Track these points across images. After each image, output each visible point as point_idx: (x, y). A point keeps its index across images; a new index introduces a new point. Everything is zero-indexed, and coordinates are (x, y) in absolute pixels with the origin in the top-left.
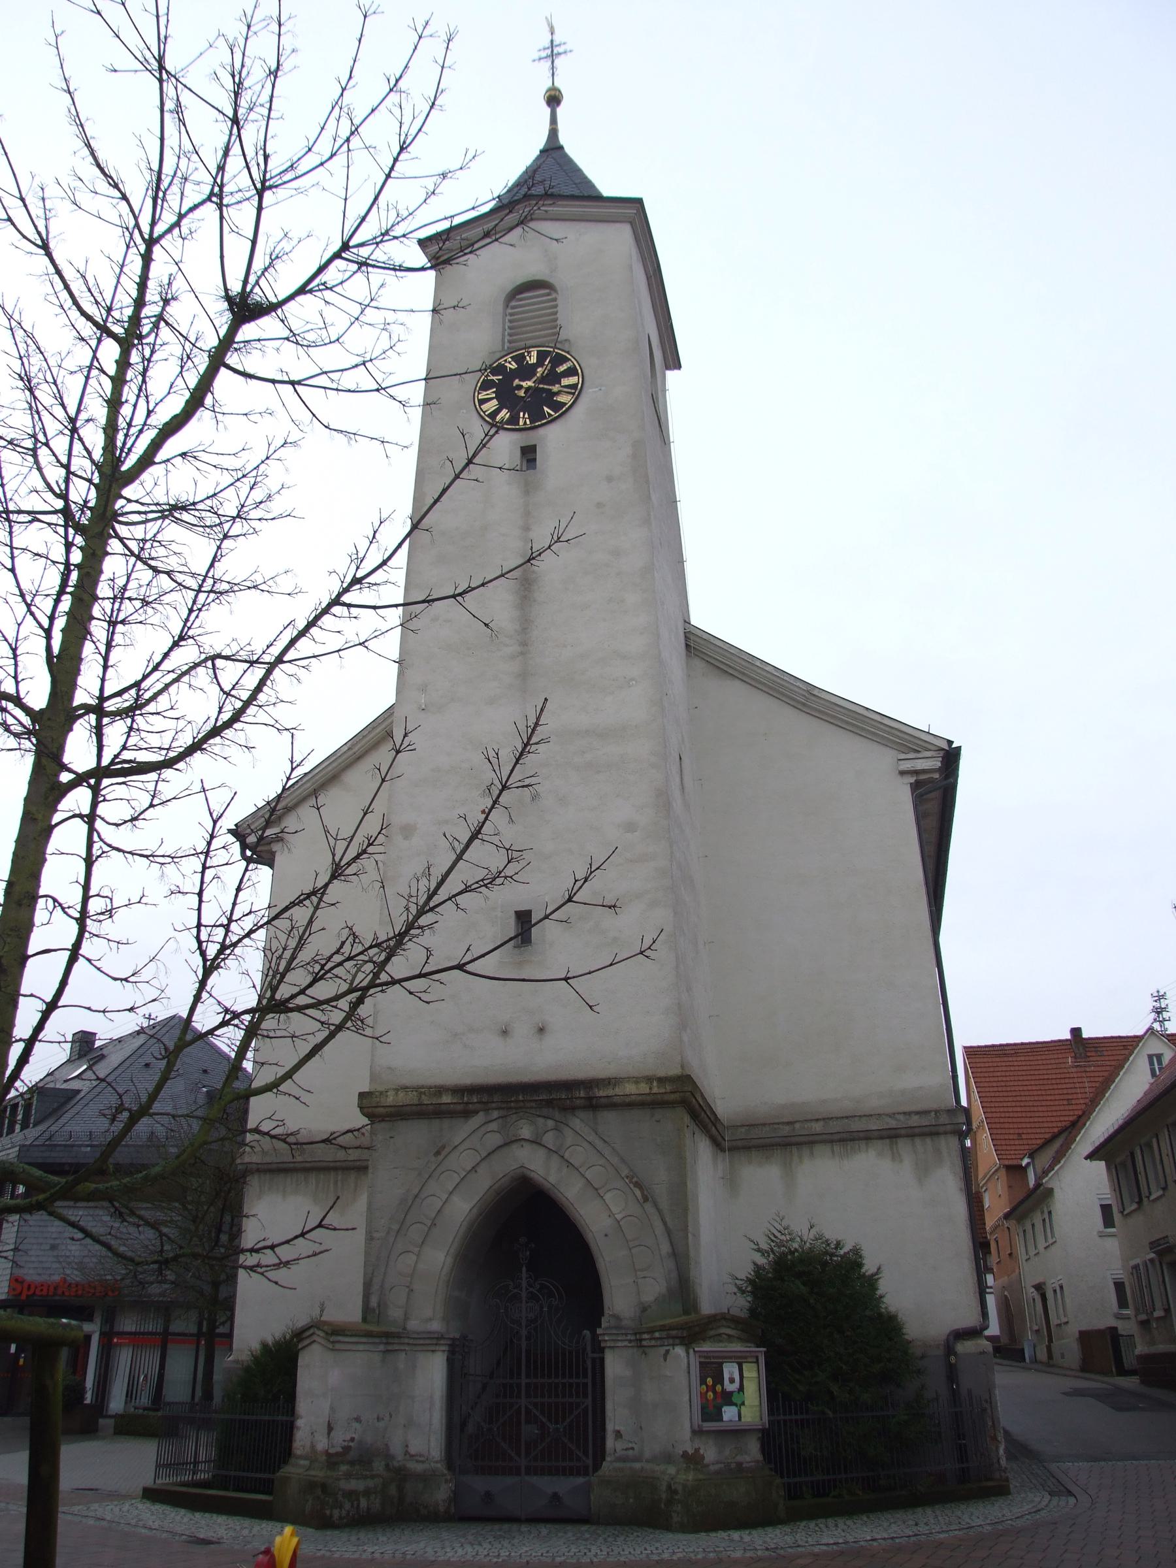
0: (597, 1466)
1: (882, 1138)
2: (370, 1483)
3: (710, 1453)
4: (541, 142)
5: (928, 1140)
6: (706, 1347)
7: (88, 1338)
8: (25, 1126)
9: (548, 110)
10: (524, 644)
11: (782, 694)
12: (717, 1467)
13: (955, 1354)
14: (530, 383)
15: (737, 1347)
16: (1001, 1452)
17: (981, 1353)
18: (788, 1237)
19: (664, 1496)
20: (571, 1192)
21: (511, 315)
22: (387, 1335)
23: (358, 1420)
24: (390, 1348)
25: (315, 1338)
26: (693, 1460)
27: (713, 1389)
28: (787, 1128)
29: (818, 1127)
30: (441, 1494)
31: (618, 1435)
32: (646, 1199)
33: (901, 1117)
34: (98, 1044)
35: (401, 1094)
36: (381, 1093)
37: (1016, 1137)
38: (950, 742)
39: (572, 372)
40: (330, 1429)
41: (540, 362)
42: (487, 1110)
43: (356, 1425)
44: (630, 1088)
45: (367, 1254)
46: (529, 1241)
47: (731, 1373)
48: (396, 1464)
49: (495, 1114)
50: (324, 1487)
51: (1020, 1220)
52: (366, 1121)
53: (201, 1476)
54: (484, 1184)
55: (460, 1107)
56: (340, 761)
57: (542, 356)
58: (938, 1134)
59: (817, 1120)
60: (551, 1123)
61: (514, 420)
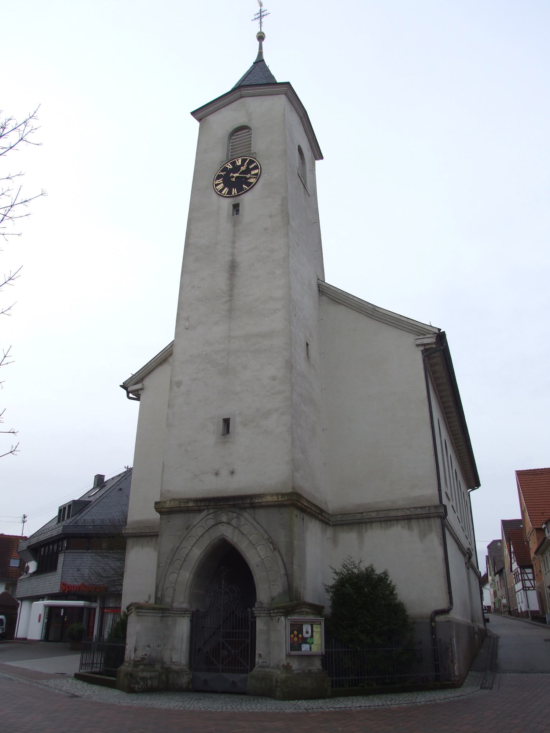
0: (251, 670)
1: (404, 519)
2: (153, 674)
3: (295, 665)
4: (254, 58)
5: (426, 520)
6: (295, 617)
7: (95, 609)
8: (68, 517)
9: (258, 43)
10: (231, 296)
11: (362, 310)
12: (298, 671)
13: (435, 622)
14: (237, 175)
15: (311, 617)
16: (455, 668)
17: (447, 621)
18: (353, 566)
19: (274, 684)
20: (243, 547)
21: (232, 143)
22: (163, 609)
23: (149, 646)
24: (164, 615)
25: (133, 610)
26: (287, 668)
27: (297, 636)
28: (360, 515)
29: (374, 515)
30: (184, 680)
31: (260, 656)
32: (275, 549)
33: (412, 510)
34: (105, 480)
35: (172, 502)
36: (164, 502)
37: (541, 514)
38: (439, 330)
39: (256, 167)
40: (136, 650)
41: (243, 165)
42: (208, 509)
43: (148, 648)
44: (269, 499)
45: (157, 573)
46: (226, 568)
47: (307, 629)
48: (166, 666)
49: (212, 511)
50: (131, 675)
51: (543, 554)
52: (158, 515)
53: (94, 670)
54: (206, 542)
55: (196, 508)
56: (167, 352)
57: (243, 161)
58: (430, 517)
59: (374, 511)
60: (235, 515)
61: (230, 192)
